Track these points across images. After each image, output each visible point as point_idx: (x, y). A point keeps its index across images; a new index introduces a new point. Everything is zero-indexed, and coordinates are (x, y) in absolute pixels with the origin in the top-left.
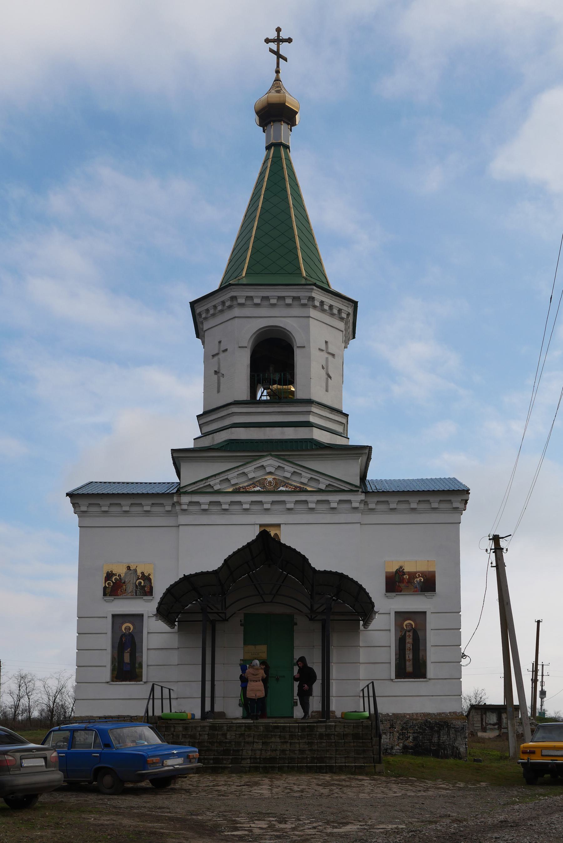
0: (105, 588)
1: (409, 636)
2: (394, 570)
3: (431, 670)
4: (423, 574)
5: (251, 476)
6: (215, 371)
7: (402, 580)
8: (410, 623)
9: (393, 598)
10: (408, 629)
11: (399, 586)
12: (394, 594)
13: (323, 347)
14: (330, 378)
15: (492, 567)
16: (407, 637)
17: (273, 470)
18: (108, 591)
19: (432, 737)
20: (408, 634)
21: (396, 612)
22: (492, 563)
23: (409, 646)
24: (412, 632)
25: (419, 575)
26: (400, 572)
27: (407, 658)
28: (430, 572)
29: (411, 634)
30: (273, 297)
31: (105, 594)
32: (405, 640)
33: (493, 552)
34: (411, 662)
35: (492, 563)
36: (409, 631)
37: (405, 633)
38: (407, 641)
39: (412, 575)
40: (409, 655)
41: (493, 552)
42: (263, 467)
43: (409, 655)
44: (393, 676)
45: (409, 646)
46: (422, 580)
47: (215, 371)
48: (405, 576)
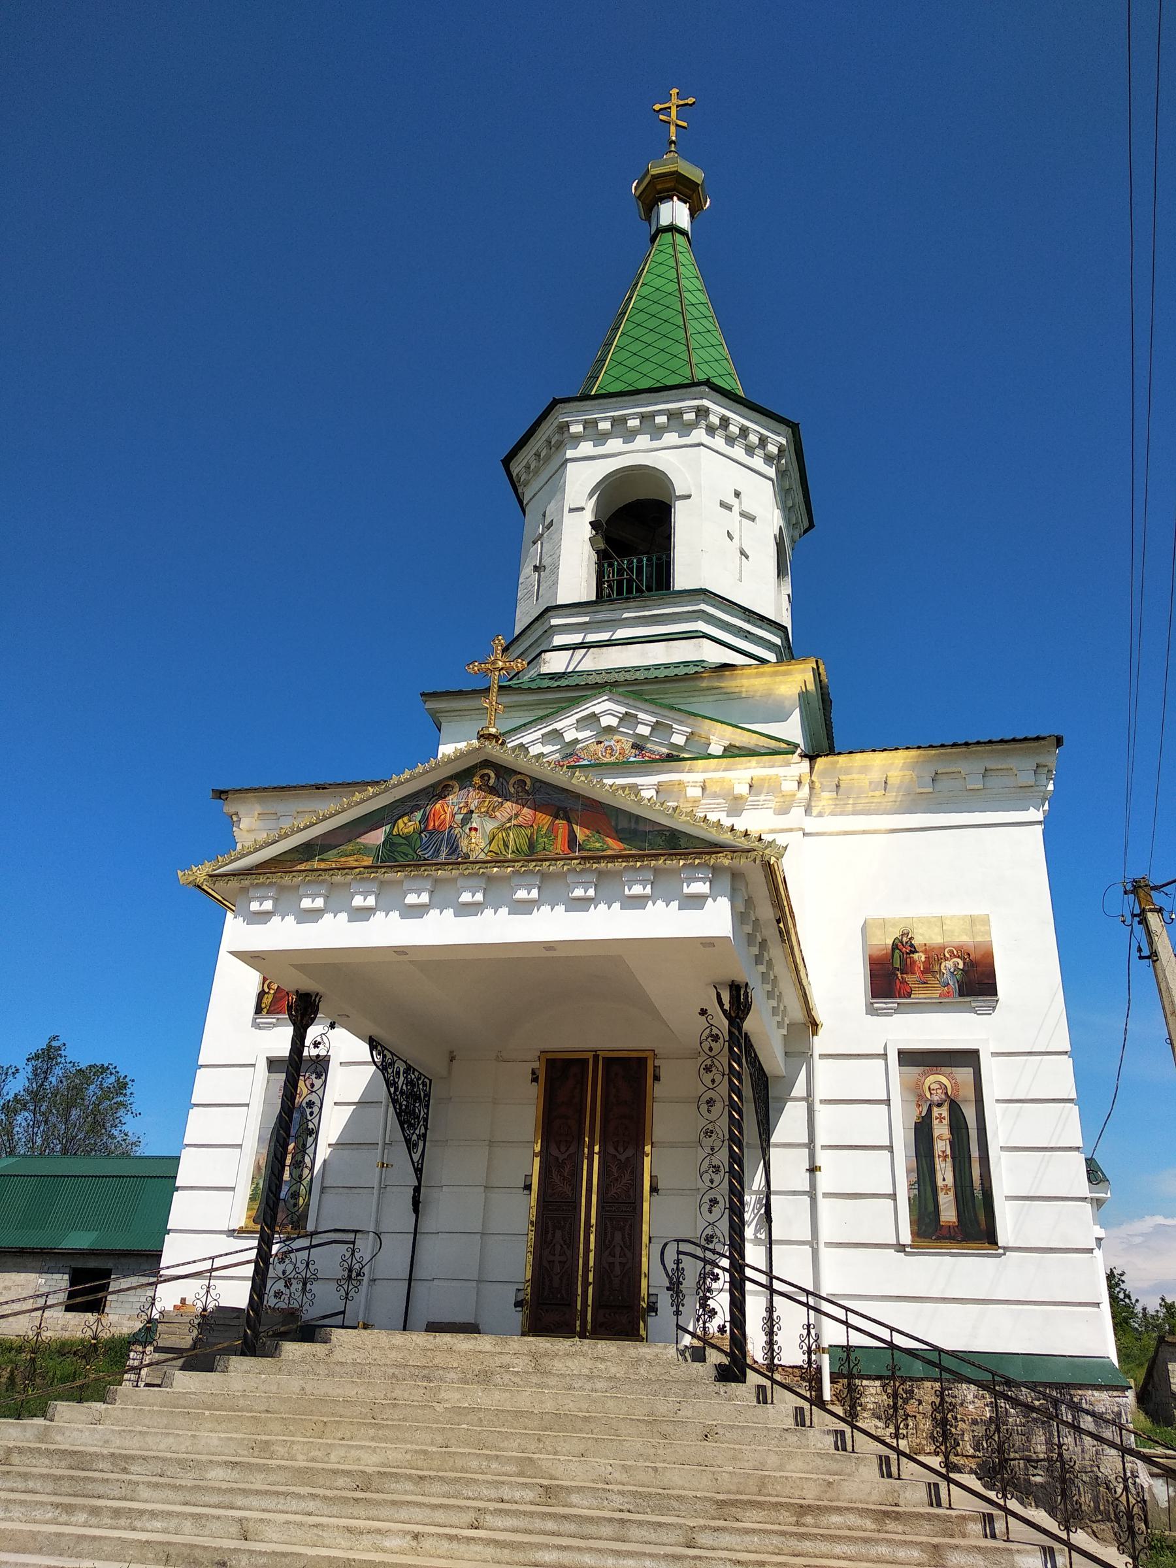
0: (261, 995)
1: (941, 1118)
2: (890, 942)
3: (1009, 1221)
4: (961, 953)
5: (569, 736)
6: (535, 567)
7: (907, 968)
8: (940, 1083)
9: (890, 1015)
10: (936, 1098)
11: (904, 982)
12: (891, 1004)
13: (731, 499)
14: (747, 557)
15: (1141, 957)
16: (936, 1122)
17: (614, 722)
18: (267, 1000)
19: (1029, 1441)
20: (936, 1111)
21: (901, 1053)
22: (1140, 950)
23: (942, 1146)
24: (946, 1106)
25: (951, 952)
26: (903, 947)
27: (940, 1183)
28: (977, 946)
29: (944, 1111)
30: (633, 416)
31: (258, 1010)
32: (931, 1129)
33: (1140, 923)
34: (952, 1194)
35: (1140, 950)
36: (939, 1105)
37: (930, 1110)
38: (936, 1133)
39: (936, 956)
40: (945, 1173)
41: (1140, 923)
42: (594, 717)
43: (945, 1173)
44: (906, 1238)
45: (942, 1146)
46: (961, 966)
47: (535, 567)
48: (916, 956)
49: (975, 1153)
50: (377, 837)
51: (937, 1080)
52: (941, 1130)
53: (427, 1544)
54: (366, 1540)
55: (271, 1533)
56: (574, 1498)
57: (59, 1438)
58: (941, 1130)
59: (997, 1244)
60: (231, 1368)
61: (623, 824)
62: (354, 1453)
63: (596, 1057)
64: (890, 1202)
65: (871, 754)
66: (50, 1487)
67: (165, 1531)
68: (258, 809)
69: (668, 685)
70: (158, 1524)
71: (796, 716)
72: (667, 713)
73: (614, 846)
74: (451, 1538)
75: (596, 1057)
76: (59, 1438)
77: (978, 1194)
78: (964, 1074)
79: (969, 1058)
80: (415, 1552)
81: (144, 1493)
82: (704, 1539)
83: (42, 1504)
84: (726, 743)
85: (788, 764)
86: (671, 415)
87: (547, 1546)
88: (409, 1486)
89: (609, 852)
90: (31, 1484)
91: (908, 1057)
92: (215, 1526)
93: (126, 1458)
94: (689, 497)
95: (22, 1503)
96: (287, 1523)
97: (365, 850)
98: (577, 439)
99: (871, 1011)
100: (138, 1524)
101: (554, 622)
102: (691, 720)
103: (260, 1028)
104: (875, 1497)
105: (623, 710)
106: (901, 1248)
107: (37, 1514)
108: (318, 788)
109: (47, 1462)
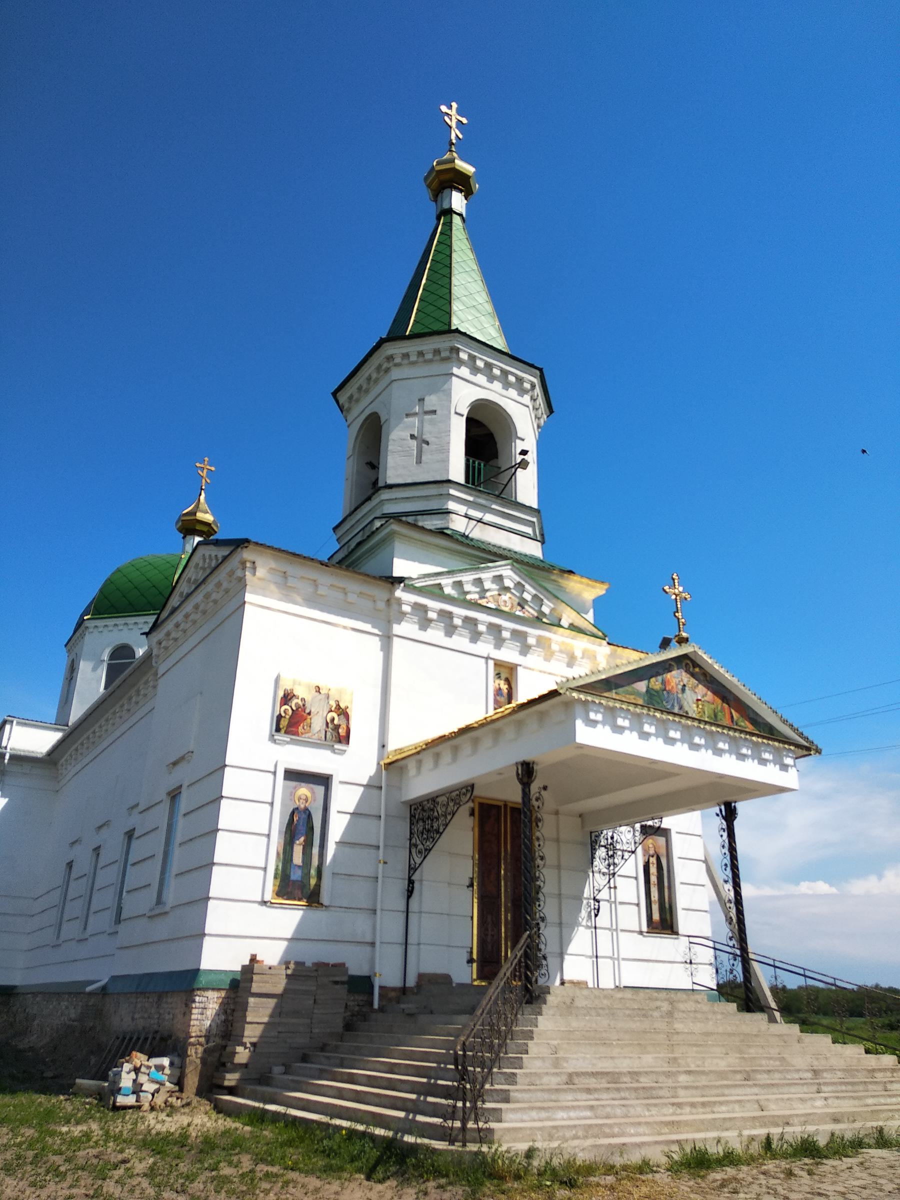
17: (511, 585)
18: (284, 723)
27: (653, 899)
49: (666, 884)
50: (642, 686)
51: (304, 790)
52: (653, 870)
53: (830, 1101)
54: (809, 1103)
55: (773, 1106)
56: (825, 1075)
57: (565, 1065)
58: (653, 870)
59: (677, 933)
60: (544, 1013)
61: (751, 715)
62: (715, 1061)
63: (506, 806)
64: (636, 908)
65: (632, 652)
66: (634, 1095)
67: (728, 1112)
68: (273, 565)
69: (536, 571)
70: (724, 1108)
71: (592, 611)
72: (542, 590)
73: (750, 728)
74: (837, 1098)
75: (506, 806)
76: (565, 1065)
77: (667, 906)
78: (661, 840)
79: (324, 781)
80: (827, 1106)
81: (681, 1092)
82: (889, 1086)
83: (666, 1104)
84: (571, 622)
85: (600, 645)
86: (505, 373)
87: (666, 1104)
88: (766, 1076)
89: (747, 730)
90: (623, 1094)
91: (293, 775)
92: (748, 1105)
93: (637, 1073)
94: (523, 440)
95: (655, 1105)
96: (777, 1099)
97: (637, 693)
98: (461, 363)
99: (272, 738)
100: (715, 1110)
101: (452, 492)
102: (555, 600)
103: (335, 753)
104: (891, 1064)
105: (518, 579)
106: (641, 933)
107: (664, 1111)
108: (322, 564)
109: (594, 1080)
